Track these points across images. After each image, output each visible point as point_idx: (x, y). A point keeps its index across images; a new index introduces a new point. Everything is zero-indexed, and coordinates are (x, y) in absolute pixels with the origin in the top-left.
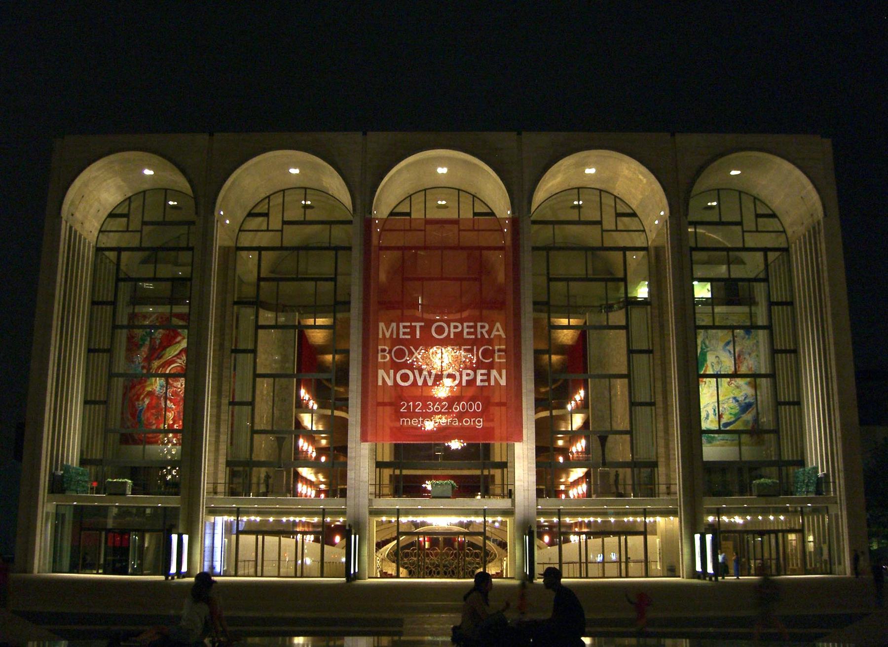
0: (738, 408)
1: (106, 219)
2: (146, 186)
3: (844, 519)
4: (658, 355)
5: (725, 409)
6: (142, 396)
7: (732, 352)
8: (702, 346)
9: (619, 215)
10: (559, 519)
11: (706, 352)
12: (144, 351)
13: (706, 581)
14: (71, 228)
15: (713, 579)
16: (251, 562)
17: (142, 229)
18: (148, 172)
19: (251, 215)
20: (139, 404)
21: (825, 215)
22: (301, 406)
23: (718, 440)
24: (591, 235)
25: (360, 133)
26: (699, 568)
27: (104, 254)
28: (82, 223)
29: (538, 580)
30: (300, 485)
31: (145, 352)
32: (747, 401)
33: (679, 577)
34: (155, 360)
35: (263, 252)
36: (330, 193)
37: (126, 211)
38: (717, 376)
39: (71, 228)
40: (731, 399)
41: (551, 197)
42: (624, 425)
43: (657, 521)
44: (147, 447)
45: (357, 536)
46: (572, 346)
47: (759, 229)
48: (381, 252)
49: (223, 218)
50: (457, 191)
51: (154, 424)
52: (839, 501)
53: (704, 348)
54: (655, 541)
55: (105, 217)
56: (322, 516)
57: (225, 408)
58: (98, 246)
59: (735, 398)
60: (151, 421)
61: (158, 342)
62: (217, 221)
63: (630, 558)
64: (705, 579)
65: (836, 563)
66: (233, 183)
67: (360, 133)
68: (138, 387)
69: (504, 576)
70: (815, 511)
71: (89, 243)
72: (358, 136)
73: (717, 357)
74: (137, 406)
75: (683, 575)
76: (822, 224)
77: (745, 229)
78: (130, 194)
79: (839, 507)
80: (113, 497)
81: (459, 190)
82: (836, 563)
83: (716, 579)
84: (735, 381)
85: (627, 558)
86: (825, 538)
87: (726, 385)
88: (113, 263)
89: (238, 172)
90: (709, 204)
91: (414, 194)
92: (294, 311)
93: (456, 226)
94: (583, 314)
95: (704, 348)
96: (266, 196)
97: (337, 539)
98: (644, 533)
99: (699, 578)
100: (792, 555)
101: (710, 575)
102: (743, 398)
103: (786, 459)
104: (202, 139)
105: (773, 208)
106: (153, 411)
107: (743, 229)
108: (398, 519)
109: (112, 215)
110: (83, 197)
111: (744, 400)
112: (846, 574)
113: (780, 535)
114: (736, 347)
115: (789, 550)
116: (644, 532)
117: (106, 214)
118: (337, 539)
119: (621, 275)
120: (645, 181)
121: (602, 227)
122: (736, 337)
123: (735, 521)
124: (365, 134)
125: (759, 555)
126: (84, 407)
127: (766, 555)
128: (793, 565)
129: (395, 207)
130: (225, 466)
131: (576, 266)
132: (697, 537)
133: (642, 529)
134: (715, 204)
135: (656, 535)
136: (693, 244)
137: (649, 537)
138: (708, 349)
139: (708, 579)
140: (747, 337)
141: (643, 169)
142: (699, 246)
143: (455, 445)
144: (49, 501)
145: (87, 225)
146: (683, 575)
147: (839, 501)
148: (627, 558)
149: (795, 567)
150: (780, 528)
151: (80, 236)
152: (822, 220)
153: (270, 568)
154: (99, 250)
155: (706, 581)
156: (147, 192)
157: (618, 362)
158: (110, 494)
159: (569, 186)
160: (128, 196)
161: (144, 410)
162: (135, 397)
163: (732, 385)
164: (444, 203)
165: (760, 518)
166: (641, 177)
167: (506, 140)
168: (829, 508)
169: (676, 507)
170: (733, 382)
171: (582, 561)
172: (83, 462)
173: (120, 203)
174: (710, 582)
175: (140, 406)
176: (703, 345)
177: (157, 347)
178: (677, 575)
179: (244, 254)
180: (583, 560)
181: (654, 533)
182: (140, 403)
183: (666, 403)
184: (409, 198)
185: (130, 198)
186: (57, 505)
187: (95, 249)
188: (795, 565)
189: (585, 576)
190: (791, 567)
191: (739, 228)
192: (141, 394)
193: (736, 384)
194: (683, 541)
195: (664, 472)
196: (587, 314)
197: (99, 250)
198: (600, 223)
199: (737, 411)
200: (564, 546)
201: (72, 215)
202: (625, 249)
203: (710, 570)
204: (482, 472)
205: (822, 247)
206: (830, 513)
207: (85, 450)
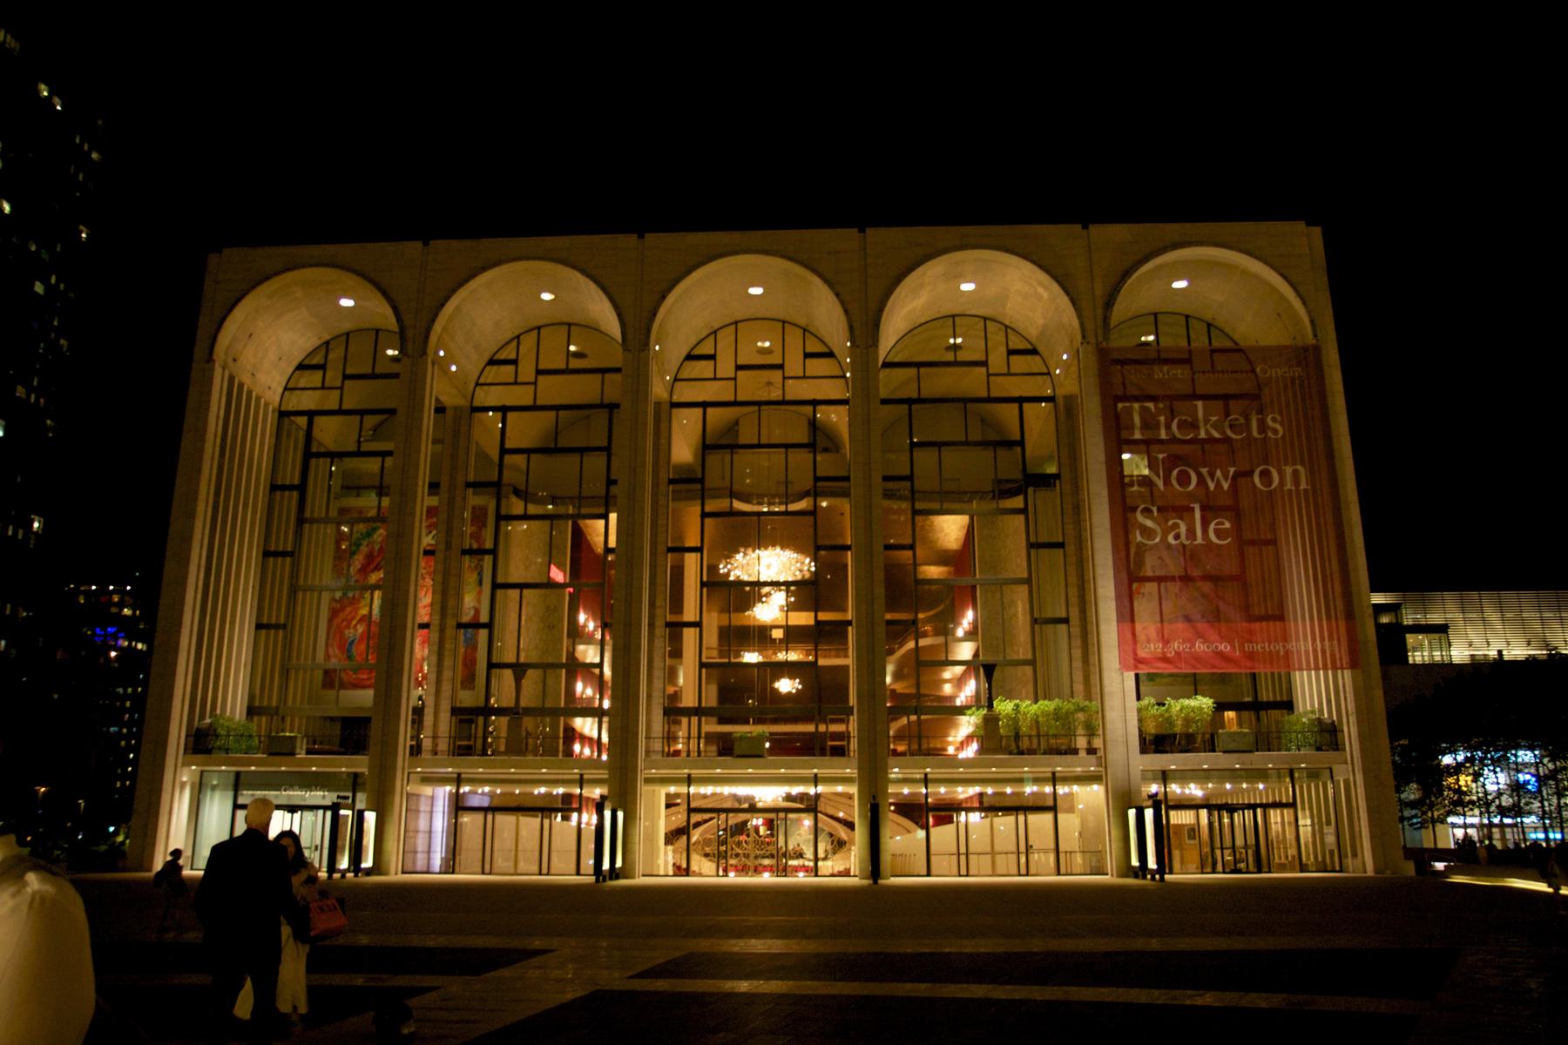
1: (294, 372)
2: (347, 326)
3: (1358, 787)
4: (1071, 548)
6: (354, 622)
9: (807, 355)
12: (358, 560)
13: (1147, 882)
15: (1157, 877)
16: (1010, 856)
17: (736, 374)
18: (346, 303)
19: (492, 362)
20: (349, 633)
22: (576, 634)
24: (972, 383)
25: (635, 236)
26: (1135, 862)
27: (294, 422)
28: (253, 375)
29: (892, 879)
30: (577, 748)
31: (358, 560)
33: (1107, 874)
34: (373, 571)
36: (603, 328)
37: (513, 356)
38: (1160, 579)
39: (232, 379)
41: (915, 328)
42: (1022, 651)
43: (1074, 791)
44: (342, 692)
45: (620, 815)
46: (956, 551)
48: (675, 411)
49: (443, 365)
52: (1349, 762)
54: (1070, 823)
55: (291, 370)
57: (450, 632)
58: (283, 409)
61: (377, 547)
62: (433, 363)
63: (1031, 846)
64: (1144, 877)
65: (1350, 855)
66: (458, 309)
67: (635, 236)
68: (348, 609)
69: (852, 874)
70: (1313, 775)
71: (267, 405)
72: (632, 239)
73: (1160, 558)
74: (346, 637)
75: (1342, 664)
78: (327, 337)
79: (1350, 769)
80: (277, 758)
81: (784, 322)
82: (1350, 855)
83: (1162, 879)
85: (1028, 847)
86: (1334, 817)
88: (303, 429)
89: (462, 293)
90: (1143, 339)
91: (721, 328)
92: (567, 504)
93: (983, 370)
94: (967, 502)
96: (514, 335)
97: (769, 832)
98: (1053, 809)
99: (1136, 876)
100: (1278, 842)
101: (1153, 873)
103: (1265, 699)
104: (413, 248)
105: (1236, 337)
107: (988, 371)
109: (301, 367)
110: (251, 335)
112: (1365, 872)
113: (1259, 811)
115: (1274, 834)
117: (295, 363)
118: (769, 832)
119: (1017, 437)
120: (1046, 295)
121: (988, 369)
123: (1191, 793)
125: (1228, 842)
126: (256, 633)
127: (1239, 842)
128: (1280, 858)
129: (692, 349)
130: (449, 714)
131: (948, 426)
133: (1050, 803)
134: (1151, 338)
136: (1120, 392)
137: (1060, 816)
139: (1149, 877)
141: (1042, 276)
143: (786, 686)
144: (186, 764)
145: (262, 378)
146: (1342, 664)
147: (1349, 762)
149: (1283, 860)
150: (1258, 802)
151: (250, 393)
153: (501, 862)
154: (283, 414)
155: (1147, 882)
156: (351, 334)
157: (1017, 565)
158: (271, 754)
159: (939, 312)
160: (324, 339)
161: (356, 641)
162: (345, 623)
164: (767, 344)
165: (1228, 786)
166: (1040, 290)
167: (845, 238)
168: (1334, 770)
171: (1021, 851)
172: (251, 711)
173: (314, 350)
174: (1154, 883)
175: (351, 635)
177: (376, 554)
178: (1105, 872)
180: (963, 850)
181: (1071, 810)
182: (352, 631)
183: (1085, 619)
184: (713, 336)
185: (327, 343)
186: (202, 772)
188: (1283, 858)
189: (965, 873)
190: (1277, 860)
192: (353, 618)
194: (1112, 826)
196: (974, 502)
197: (283, 414)
201: (235, 360)
202: (1020, 401)
203: (1152, 864)
204: (817, 728)
206: (1335, 779)
207: (258, 692)
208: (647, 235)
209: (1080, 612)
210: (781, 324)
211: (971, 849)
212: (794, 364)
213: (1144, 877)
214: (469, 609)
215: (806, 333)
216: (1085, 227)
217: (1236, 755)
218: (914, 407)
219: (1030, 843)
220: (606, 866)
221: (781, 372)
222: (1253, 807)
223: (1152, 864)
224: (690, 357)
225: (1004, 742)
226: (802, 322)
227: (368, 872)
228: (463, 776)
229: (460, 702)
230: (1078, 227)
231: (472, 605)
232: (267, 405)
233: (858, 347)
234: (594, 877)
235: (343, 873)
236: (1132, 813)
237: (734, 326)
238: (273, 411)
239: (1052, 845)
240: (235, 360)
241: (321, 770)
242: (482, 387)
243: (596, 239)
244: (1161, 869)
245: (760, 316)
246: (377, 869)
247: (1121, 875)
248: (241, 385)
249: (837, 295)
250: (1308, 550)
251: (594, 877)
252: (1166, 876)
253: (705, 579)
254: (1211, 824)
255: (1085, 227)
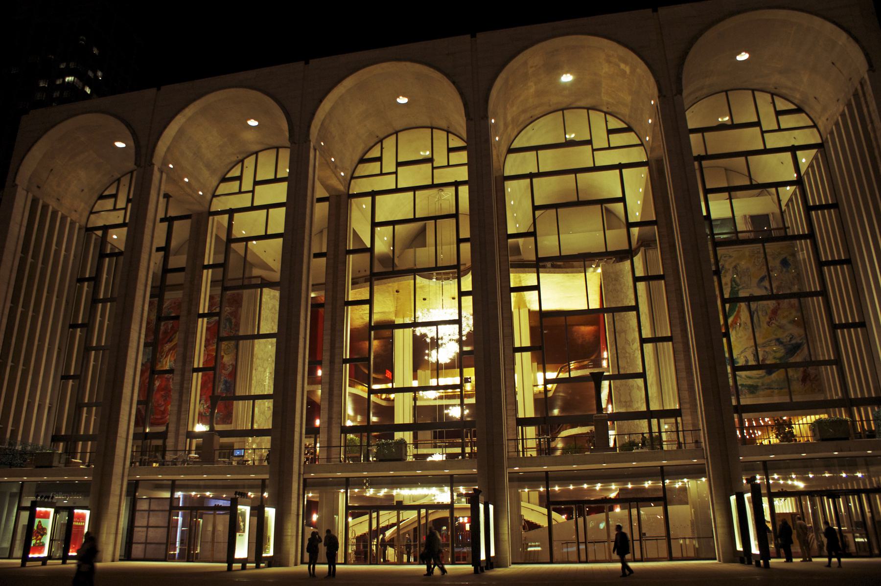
0: (783, 351)
5: (767, 352)
7: (769, 288)
8: (732, 285)
10: (547, 488)
11: (738, 290)
14: (35, 201)
19: (102, 197)
21: (871, 68)
23: (763, 390)
25: (468, 37)
32: (793, 342)
33: (715, 559)
34: (167, 343)
35: (624, 171)
40: (774, 341)
45: (491, 507)
47: (782, 127)
50: (586, 110)
51: (163, 405)
53: (735, 286)
56: (170, 489)
59: (778, 340)
60: (160, 402)
64: (750, 563)
67: (304, 62)
71: (72, 223)
72: (300, 65)
76: (868, 82)
77: (764, 129)
83: (767, 564)
84: (776, 320)
87: (765, 326)
95: (735, 286)
99: (742, 561)
102: (788, 339)
104: (150, 93)
106: (162, 393)
108: (548, 490)
111: (790, 341)
114: (772, 283)
116: (663, 499)
122: (772, 271)
124: (473, 36)
132: (733, 499)
133: (661, 494)
134: (727, 118)
135: (688, 504)
138: (740, 287)
139: (754, 563)
140: (784, 270)
142: (709, 153)
148: (642, 535)
151: (55, 213)
152: (866, 76)
158: (37, 467)
163: (773, 325)
166: (622, 66)
169: (702, 461)
170: (774, 321)
176: (733, 283)
177: (169, 331)
179: (216, 218)
187: (83, 231)
191: (757, 130)
193: (777, 323)
195: (690, 422)
198: (758, 124)
199: (783, 355)
200: (610, 513)
203: (755, 550)
205: (871, 109)
208: (311, 61)
209: (682, 330)
210: (430, 129)
211: (589, 539)
212: (600, 140)
213: (750, 563)
214: (229, 366)
215: (775, 97)
216: (655, 10)
217: (835, 442)
218: (535, 180)
219: (643, 531)
220: (483, 557)
221: (430, 164)
222: (857, 492)
223: (755, 550)
224: (363, 161)
225: (465, 349)
226: (445, 126)
227: (271, 562)
228: (177, 482)
229: (626, 516)
230: (649, 11)
231: (231, 363)
232: (72, 223)
233: (472, 120)
234: (226, 565)
235: (244, 562)
236: (733, 499)
237: (395, 136)
238: (80, 229)
239: (663, 533)
240: (39, 187)
241: (51, 479)
242: (218, 198)
243: (274, 69)
244: (765, 553)
245: (414, 125)
246: (277, 560)
247: (726, 561)
248: (45, 207)
249: (454, 83)
250: (853, 365)
251: (226, 565)
252: (772, 561)
253: (131, 197)
254: (814, 513)
255: (655, 10)
